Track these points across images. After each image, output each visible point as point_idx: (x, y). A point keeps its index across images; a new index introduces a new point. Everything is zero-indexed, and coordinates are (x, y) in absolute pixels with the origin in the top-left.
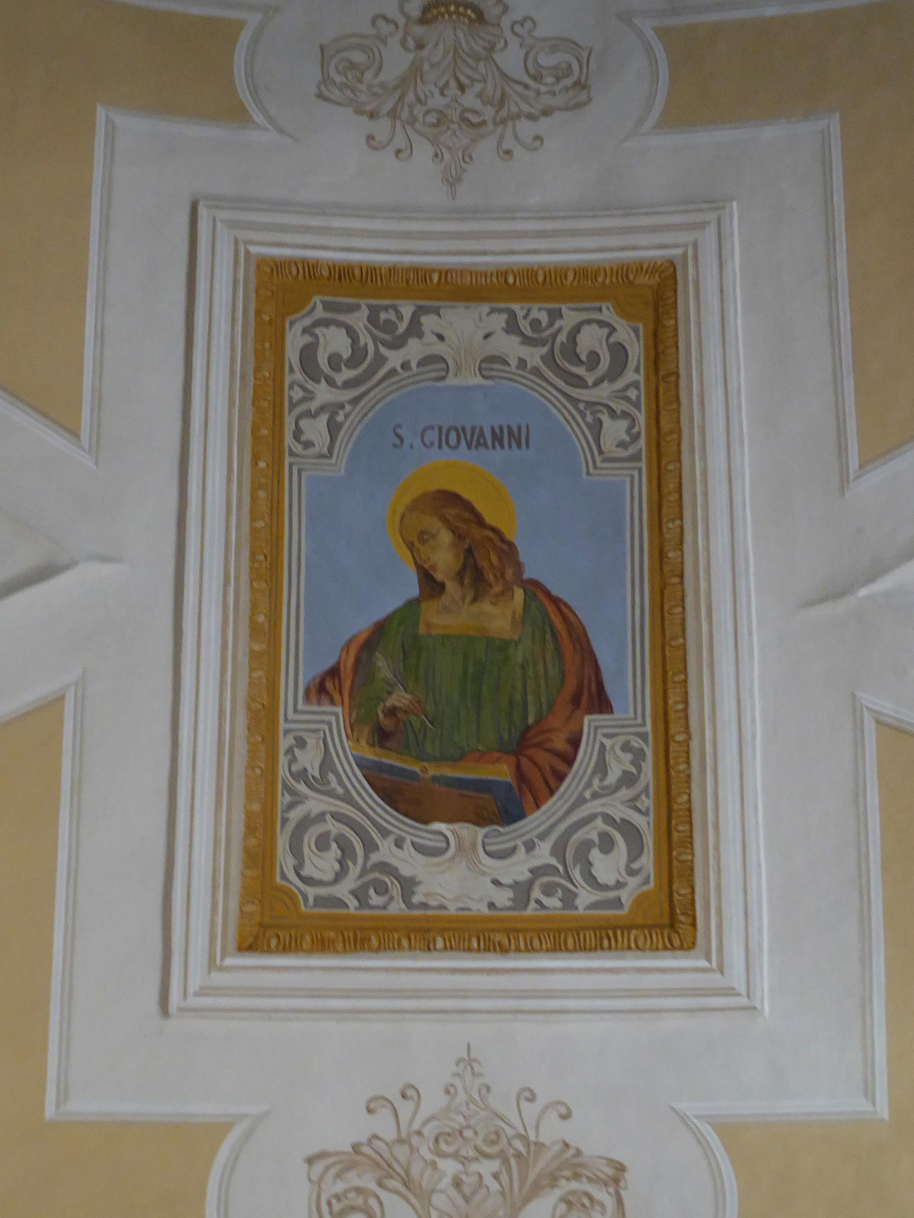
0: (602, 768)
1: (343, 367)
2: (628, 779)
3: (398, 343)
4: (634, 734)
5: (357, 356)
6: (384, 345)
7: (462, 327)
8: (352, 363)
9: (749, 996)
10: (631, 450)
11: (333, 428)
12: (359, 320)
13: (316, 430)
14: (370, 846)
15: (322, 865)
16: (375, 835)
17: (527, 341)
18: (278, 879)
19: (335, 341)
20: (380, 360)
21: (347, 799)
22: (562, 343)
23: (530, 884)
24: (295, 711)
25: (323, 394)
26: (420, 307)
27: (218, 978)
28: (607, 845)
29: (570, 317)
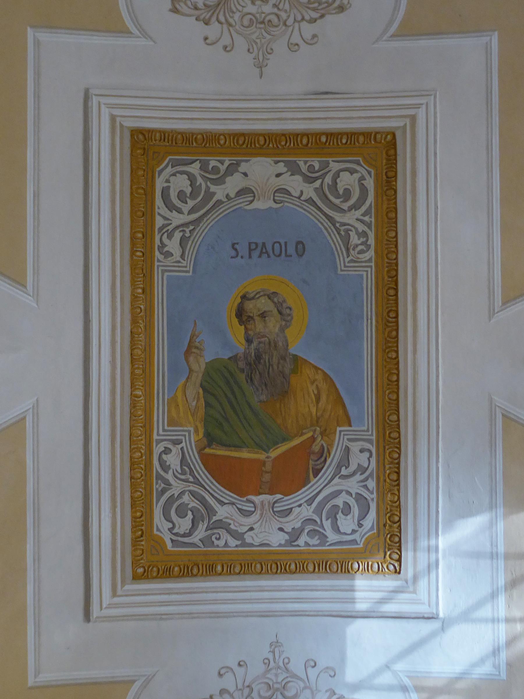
3: (220, 181)
4: (162, 262)
5: (333, 516)
6: (315, 521)
7: (261, 170)
8: (193, 195)
9: (99, 103)
11: (183, 242)
12: (195, 169)
13: (173, 245)
15: (346, 180)
16: (316, 199)
18: (155, 532)
20: (319, 511)
23: (302, 530)
27: (116, 600)
28: (181, 195)
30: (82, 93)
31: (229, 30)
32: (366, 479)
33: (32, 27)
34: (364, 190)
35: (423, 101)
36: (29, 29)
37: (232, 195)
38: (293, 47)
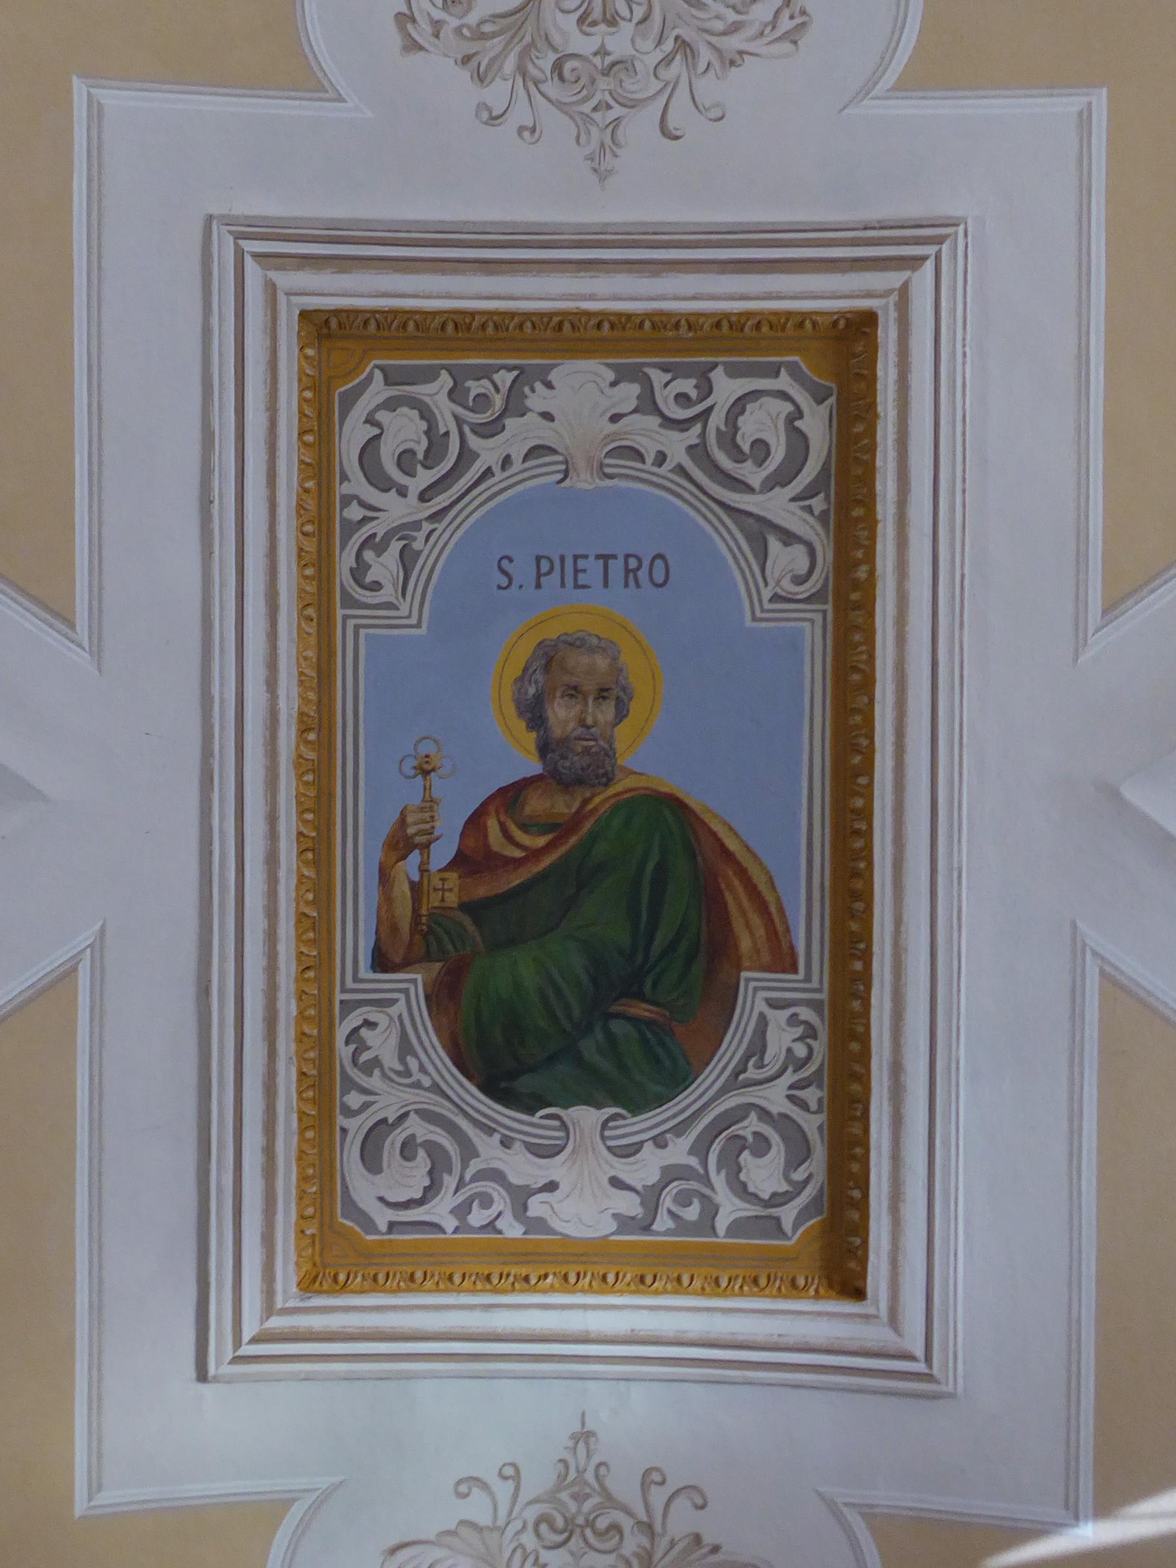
0: (758, 1047)
1: (750, 1138)
2: (792, 1062)
5: (436, 443)
7: (580, 397)
8: (432, 456)
10: (355, 1019)
11: (407, 558)
12: (436, 392)
14: (469, 1152)
17: (497, 1176)
19: (404, 430)
20: (466, 456)
21: (436, 1088)
22: (450, 1173)
24: (356, 979)
25: (395, 510)
26: (647, 1229)
29: (726, 388)
30: (171, 202)
31: (649, 1516)
32: (365, 520)
33: (79, 76)
34: (798, 441)
35: (930, 250)
36: (75, 79)
37: (649, 1147)
38: (513, 1474)
